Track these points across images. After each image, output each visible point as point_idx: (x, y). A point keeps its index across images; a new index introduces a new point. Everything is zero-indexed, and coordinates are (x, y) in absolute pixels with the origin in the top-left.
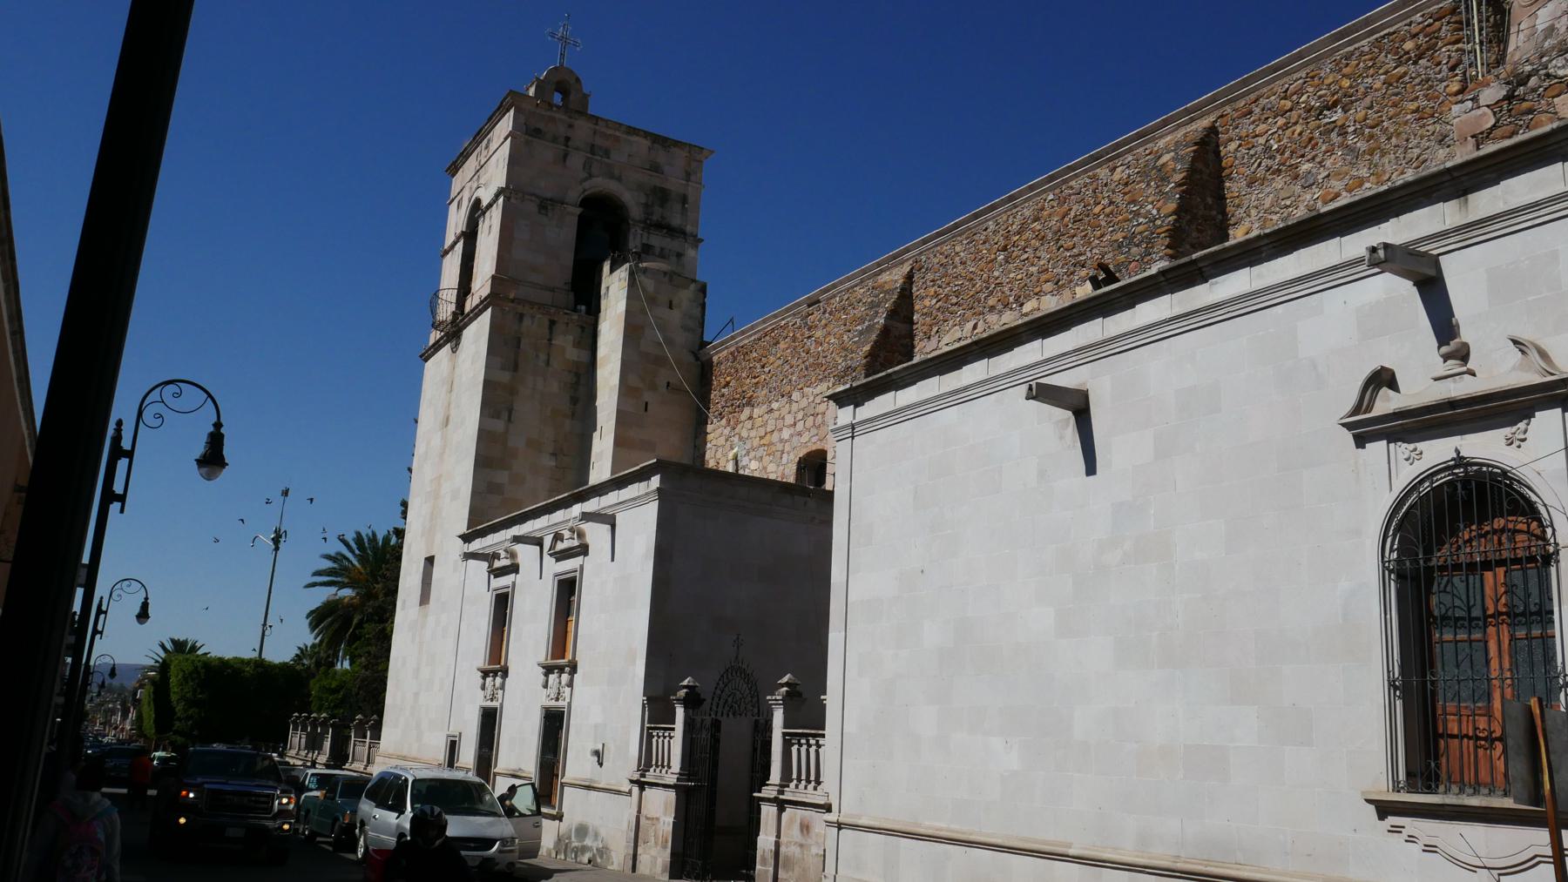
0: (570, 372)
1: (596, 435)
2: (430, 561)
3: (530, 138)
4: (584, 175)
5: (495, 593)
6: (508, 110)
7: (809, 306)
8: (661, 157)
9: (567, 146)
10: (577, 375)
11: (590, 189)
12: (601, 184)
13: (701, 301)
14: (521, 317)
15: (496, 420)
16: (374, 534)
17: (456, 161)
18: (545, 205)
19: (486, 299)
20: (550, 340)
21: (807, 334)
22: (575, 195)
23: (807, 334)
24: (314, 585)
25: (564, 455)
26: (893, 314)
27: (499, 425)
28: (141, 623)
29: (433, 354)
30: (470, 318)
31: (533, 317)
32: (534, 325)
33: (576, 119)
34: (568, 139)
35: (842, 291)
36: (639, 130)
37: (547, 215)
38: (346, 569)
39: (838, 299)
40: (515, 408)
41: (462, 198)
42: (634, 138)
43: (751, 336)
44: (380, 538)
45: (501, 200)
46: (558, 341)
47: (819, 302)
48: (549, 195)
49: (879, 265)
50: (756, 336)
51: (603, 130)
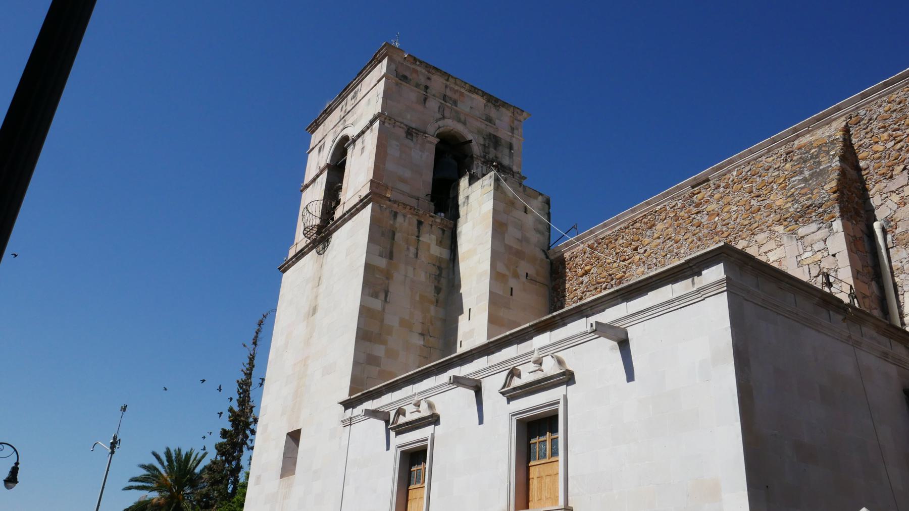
0: (434, 265)
1: (463, 321)
2: (294, 436)
3: (400, 81)
4: (439, 116)
5: (399, 450)
6: (380, 62)
7: (693, 187)
8: (493, 113)
9: (427, 92)
10: (440, 268)
11: (443, 127)
12: (451, 125)
13: (547, 212)
14: (395, 215)
15: (374, 299)
16: (179, 450)
17: (318, 119)
18: (410, 132)
19: (366, 197)
20: (418, 237)
21: (694, 210)
22: (432, 129)
23: (694, 210)
24: (130, 488)
25: (431, 337)
26: (843, 159)
27: (377, 304)
28: (8, 488)
29: (294, 263)
30: (345, 219)
31: (405, 216)
32: (405, 223)
33: (433, 74)
34: (427, 87)
35: (741, 165)
36: (479, 90)
37: (412, 140)
38: (156, 477)
39: (735, 173)
40: (390, 290)
41: (324, 143)
42: (475, 96)
43: (615, 227)
44: (183, 453)
45: (377, 124)
46: (425, 238)
47: (708, 180)
48: (414, 126)
49: (795, 130)
50: (622, 226)
51: (453, 86)
